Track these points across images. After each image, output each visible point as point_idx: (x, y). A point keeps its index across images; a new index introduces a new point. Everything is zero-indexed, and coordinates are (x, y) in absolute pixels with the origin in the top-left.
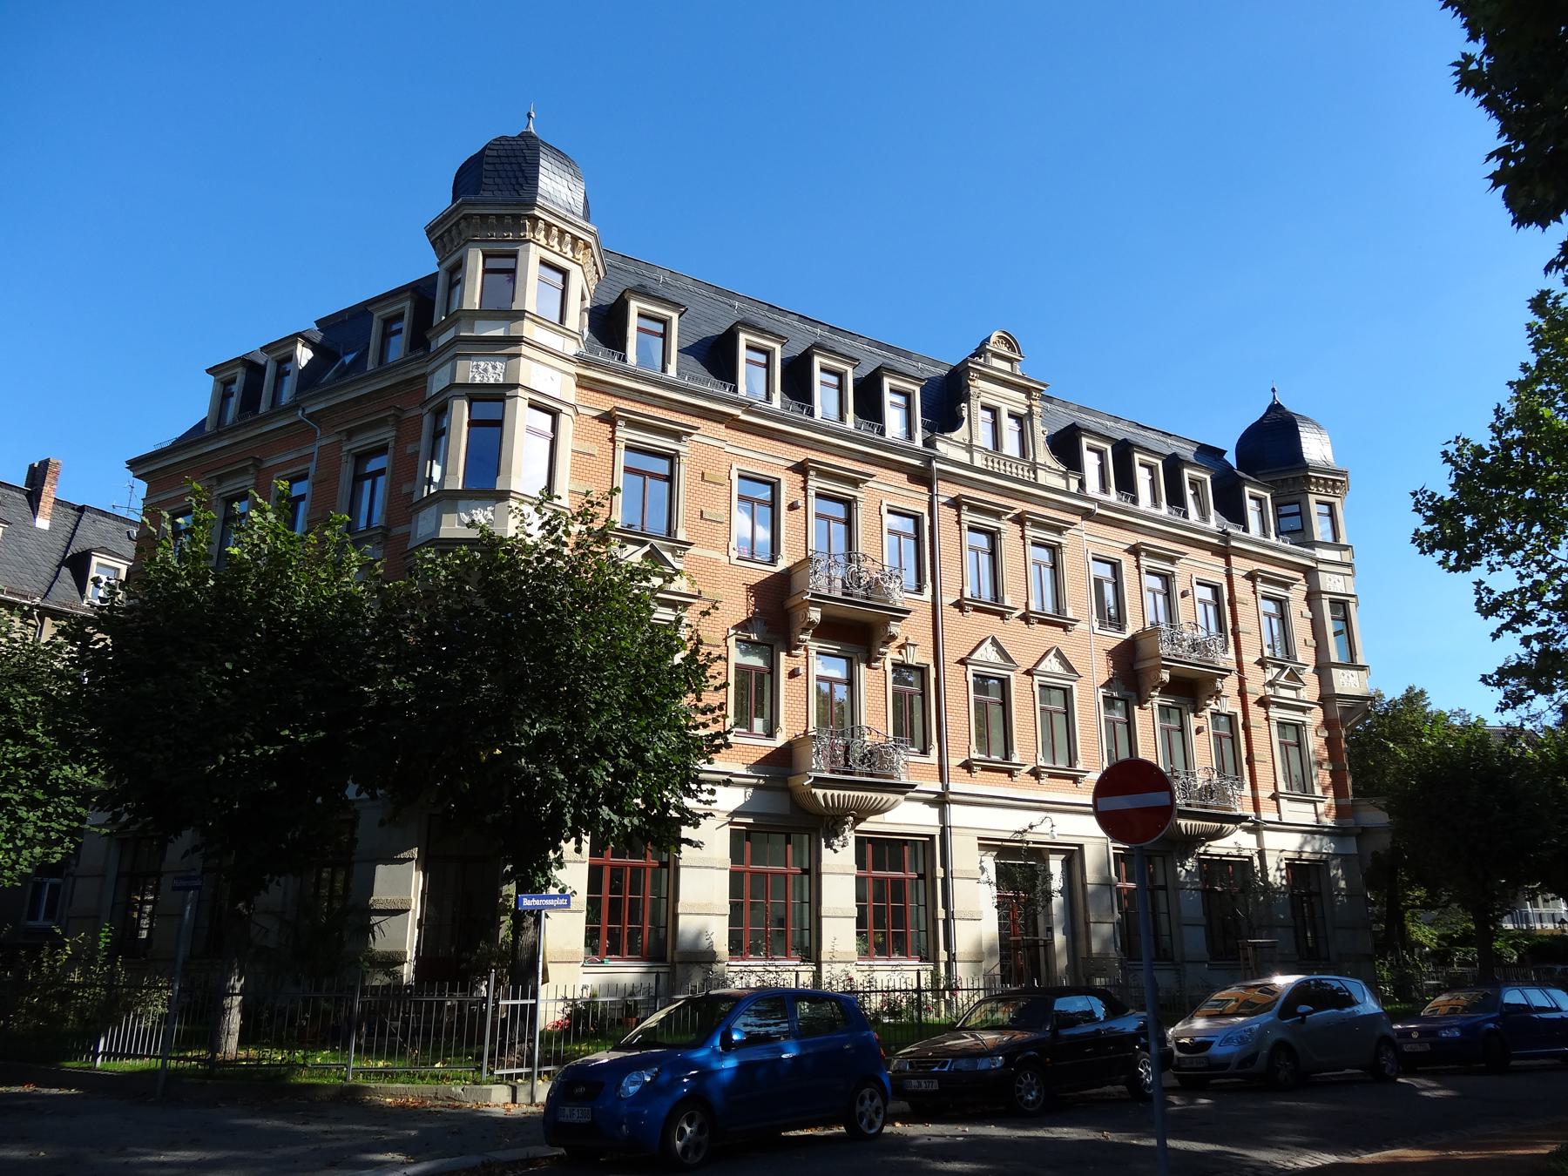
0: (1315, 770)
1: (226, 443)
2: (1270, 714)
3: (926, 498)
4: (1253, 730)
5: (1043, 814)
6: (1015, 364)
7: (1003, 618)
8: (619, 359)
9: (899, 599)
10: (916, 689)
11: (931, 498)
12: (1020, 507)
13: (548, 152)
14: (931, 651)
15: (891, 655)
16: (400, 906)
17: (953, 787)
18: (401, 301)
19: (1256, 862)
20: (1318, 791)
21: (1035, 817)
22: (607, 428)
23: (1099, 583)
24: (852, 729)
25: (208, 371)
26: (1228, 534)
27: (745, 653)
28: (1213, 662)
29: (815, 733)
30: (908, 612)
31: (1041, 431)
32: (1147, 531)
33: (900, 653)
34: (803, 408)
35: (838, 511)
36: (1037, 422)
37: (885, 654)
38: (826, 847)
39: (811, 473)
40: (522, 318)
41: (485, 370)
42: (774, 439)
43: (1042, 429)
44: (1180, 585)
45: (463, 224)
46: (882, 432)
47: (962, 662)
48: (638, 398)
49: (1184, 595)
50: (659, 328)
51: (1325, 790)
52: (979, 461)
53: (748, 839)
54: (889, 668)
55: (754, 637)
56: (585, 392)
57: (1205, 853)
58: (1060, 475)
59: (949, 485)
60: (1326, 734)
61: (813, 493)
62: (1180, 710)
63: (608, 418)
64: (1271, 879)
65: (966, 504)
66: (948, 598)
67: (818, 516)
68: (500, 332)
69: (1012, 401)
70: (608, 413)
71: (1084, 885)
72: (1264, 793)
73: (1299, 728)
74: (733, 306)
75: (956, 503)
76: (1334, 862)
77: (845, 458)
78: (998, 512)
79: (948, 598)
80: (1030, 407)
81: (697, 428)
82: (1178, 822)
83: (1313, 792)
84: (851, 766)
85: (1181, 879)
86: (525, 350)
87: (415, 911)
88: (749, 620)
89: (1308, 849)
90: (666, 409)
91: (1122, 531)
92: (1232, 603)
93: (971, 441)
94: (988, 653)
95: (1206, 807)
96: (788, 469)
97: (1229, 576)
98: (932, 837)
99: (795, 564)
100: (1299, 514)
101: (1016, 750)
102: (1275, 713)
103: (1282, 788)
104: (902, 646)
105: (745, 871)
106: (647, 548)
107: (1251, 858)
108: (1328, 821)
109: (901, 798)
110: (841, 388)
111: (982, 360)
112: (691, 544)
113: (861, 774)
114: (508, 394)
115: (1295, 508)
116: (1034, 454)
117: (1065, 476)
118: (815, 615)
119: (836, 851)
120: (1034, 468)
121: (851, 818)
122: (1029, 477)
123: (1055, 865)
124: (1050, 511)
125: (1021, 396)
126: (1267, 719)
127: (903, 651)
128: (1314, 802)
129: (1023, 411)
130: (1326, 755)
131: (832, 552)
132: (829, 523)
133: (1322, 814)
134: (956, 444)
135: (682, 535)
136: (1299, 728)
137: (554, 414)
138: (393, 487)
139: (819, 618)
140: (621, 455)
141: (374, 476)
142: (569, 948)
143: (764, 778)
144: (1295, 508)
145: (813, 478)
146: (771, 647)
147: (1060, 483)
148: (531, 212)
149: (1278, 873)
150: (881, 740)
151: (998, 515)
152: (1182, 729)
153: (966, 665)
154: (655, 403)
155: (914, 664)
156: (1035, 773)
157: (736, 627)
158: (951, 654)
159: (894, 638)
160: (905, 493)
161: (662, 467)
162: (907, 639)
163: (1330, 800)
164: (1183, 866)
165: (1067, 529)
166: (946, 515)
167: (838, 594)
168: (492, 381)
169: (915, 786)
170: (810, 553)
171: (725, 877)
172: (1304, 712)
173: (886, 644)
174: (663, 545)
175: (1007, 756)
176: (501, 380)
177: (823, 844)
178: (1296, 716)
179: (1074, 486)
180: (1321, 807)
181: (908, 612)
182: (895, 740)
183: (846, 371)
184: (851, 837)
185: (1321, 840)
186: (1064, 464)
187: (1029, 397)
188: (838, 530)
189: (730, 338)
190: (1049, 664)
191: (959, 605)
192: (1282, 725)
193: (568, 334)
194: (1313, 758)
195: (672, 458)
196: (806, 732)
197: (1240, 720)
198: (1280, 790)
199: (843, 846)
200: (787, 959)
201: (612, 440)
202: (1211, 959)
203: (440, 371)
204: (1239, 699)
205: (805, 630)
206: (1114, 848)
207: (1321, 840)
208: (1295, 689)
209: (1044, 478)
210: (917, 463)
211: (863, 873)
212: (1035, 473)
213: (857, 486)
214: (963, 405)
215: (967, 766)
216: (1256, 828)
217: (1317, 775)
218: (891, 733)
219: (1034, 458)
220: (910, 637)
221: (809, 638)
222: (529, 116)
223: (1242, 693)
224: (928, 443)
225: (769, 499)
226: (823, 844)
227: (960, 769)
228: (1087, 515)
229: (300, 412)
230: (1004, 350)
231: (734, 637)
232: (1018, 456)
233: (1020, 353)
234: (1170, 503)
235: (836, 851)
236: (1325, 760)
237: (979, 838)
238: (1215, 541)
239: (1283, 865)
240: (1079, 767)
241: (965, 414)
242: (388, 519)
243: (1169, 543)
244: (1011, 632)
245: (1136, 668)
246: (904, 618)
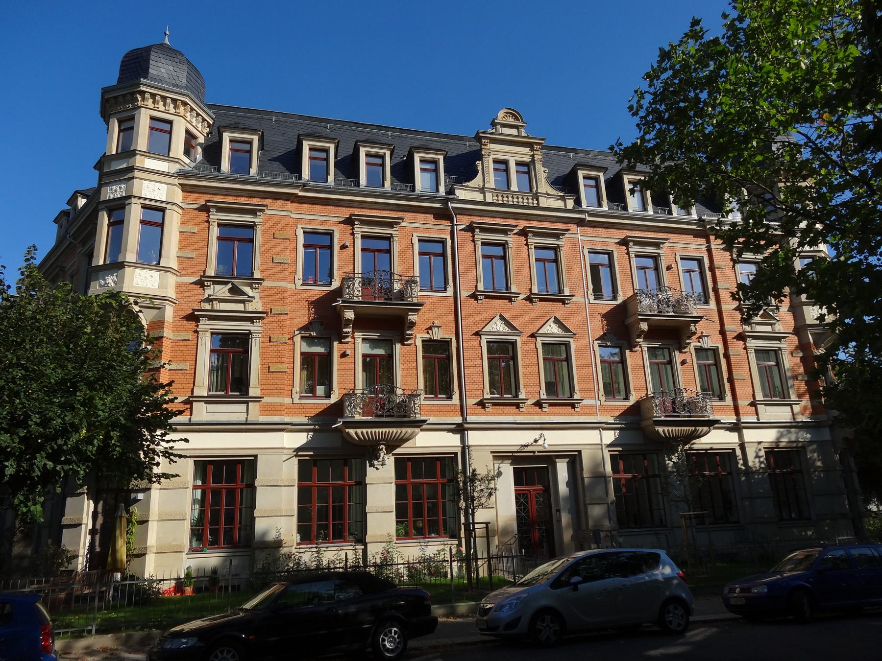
0: (790, 382)
2: (747, 345)
3: (449, 228)
4: (732, 359)
5: (539, 432)
6: (520, 129)
7: (510, 301)
8: (296, 178)
9: (696, 309)
10: (711, 361)
11: (452, 228)
12: (521, 224)
13: (157, 51)
14: (453, 329)
15: (693, 343)
16: (77, 522)
17: (470, 419)
19: (738, 452)
20: (793, 397)
21: (536, 434)
22: (523, 238)
23: (595, 269)
24: (675, 391)
26: (704, 221)
27: (310, 345)
28: (687, 313)
29: (652, 395)
30: (421, 305)
32: (635, 228)
33: (699, 342)
34: (665, 210)
35: (650, 263)
36: (539, 166)
37: (690, 343)
38: (370, 466)
39: (529, 235)
40: (135, 155)
41: (116, 191)
42: (328, 205)
43: (543, 169)
44: (664, 264)
46: (413, 189)
47: (533, 336)
48: (506, 216)
49: (669, 268)
50: (379, 161)
51: (800, 396)
52: (489, 199)
53: (315, 465)
54: (693, 351)
55: (314, 334)
56: (189, 194)
57: (691, 449)
58: (558, 199)
59: (465, 217)
60: (801, 355)
61: (633, 255)
62: (669, 349)
63: (205, 209)
64: (750, 464)
65: (478, 227)
66: (465, 293)
67: (684, 271)
68: (124, 166)
69: (515, 155)
70: (205, 205)
71: (583, 479)
72: (743, 402)
73: (777, 352)
74: (569, 157)
75: (470, 228)
76: (811, 448)
77: (384, 210)
78: (557, 234)
79: (465, 293)
80: (533, 156)
81: (568, 230)
82: (656, 429)
83: (790, 398)
84: (677, 412)
85: (669, 469)
86: (137, 174)
87: (87, 525)
88: (605, 334)
89: (785, 439)
90: (247, 197)
91: (614, 230)
92: (712, 269)
93: (484, 185)
94: (498, 326)
95: (690, 416)
96: (340, 223)
97: (709, 251)
98: (456, 454)
99: (628, 298)
101: (522, 390)
102: (752, 344)
103: (759, 396)
104: (700, 338)
105: (408, 484)
106: (230, 286)
107: (734, 450)
108: (801, 418)
109: (417, 430)
110: (597, 187)
111: (494, 131)
112: (573, 296)
113: (685, 416)
114: (126, 202)
116: (537, 187)
117: (562, 199)
118: (644, 327)
119: (377, 469)
120: (536, 196)
121: (383, 446)
122: (533, 204)
123: (562, 469)
124: (550, 224)
125: (527, 150)
126: (745, 348)
127: (701, 340)
128: (791, 405)
129: (528, 159)
130: (801, 370)
131: (649, 289)
132: (645, 271)
133: (797, 414)
134: (473, 189)
135: (257, 275)
136: (777, 352)
139: (354, 317)
140: (533, 252)
142: (175, 543)
143: (318, 425)
145: (359, 226)
146: (620, 348)
147: (560, 204)
148: (139, 89)
149: (757, 460)
150: (694, 395)
151: (505, 232)
152: (670, 362)
153: (535, 337)
154: (237, 194)
155: (439, 339)
156: (539, 404)
157: (300, 329)
158: (466, 331)
159: (694, 333)
160: (431, 227)
161: (499, 251)
162: (702, 333)
163: (806, 401)
164: (670, 459)
165: (663, 243)
166: (463, 238)
167: (656, 313)
168: (119, 196)
169: (426, 421)
170: (636, 291)
171: (393, 487)
172: (780, 341)
173: (689, 338)
174: (238, 282)
175: (571, 396)
176: (124, 195)
177: (368, 464)
178: (774, 344)
179: (570, 204)
180: (797, 409)
181: (421, 305)
182: (702, 394)
183: (599, 176)
184: (390, 461)
185: (797, 433)
186: (561, 190)
187: (532, 149)
188: (651, 274)
189: (573, 174)
190: (548, 328)
191: (474, 296)
192: (761, 353)
194: (789, 374)
195: (556, 249)
196: (647, 394)
197: (721, 351)
198: (757, 399)
199: (382, 465)
200: (439, 537)
201: (527, 245)
202: (620, 528)
204: (720, 337)
205: (639, 336)
206: (609, 451)
207: (797, 433)
208: (243, 302)
209: (544, 202)
210: (438, 205)
211: (617, 476)
212: (538, 200)
213: (393, 227)
214: (477, 162)
215: (482, 404)
216: (736, 428)
217: (793, 386)
218: (699, 390)
219: (537, 190)
220: (704, 331)
221: (642, 340)
222: (166, 34)
223: (723, 332)
224: (450, 192)
225: (608, 263)
226: (368, 464)
227: (476, 407)
228: (581, 223)
230: (511, 121)
231: (299, 336)
233: (522, 121)
234: (655, 203)
235: (377, 469)
236: (800, 374)
237: (492, 452)
238: (694, 227)
239: (762, 453)
240: (576, 397)
241: (480, 168)
243: (655, 234)
244: (518, 310)
245: (626, 323)
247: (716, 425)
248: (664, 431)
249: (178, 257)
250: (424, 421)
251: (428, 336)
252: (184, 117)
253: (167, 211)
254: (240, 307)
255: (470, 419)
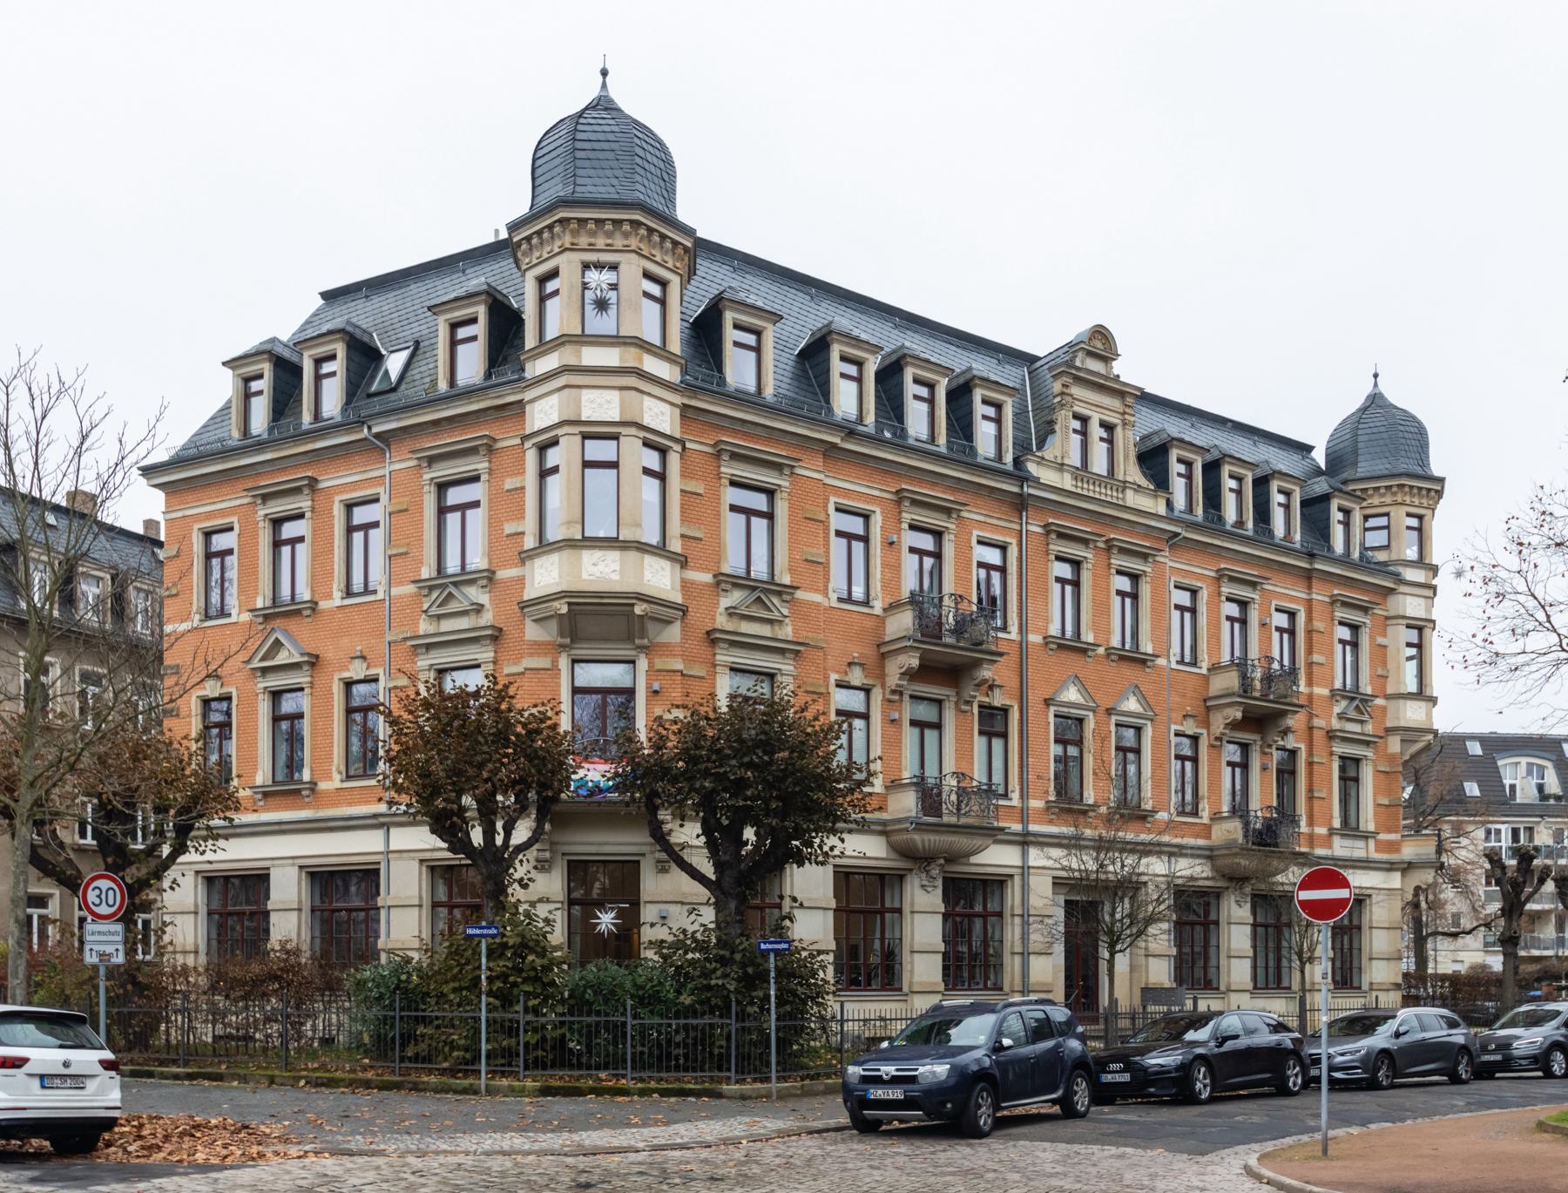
1: (268, 456)
18: (475, 304)
25: (224, 364)
30: (1001, 654)
31: (1127, 441)
45: (557, 229)
100: (1387, 527)
115: (1383, 521)
137: (663, 452)
138: (493, 524)
141: (463, 508)
144: (1383, 521)
158: (1035, 697)
181: (1001, 654)
193: (669, 357)
203: (543, 401)
208: (770, 622)
209: (1132, 499)
229: (366, 430)
232: (1079, 465)
242: (490, 556)
246: (996, 661)
247: (999, 837)
248: (923, 840)
249: (682, 536)
250: (1002, 829)
251: (987, 700)
252: (1396, 504)
253: (622, 439)
254: (765, 630)
255: (1033, 828)
